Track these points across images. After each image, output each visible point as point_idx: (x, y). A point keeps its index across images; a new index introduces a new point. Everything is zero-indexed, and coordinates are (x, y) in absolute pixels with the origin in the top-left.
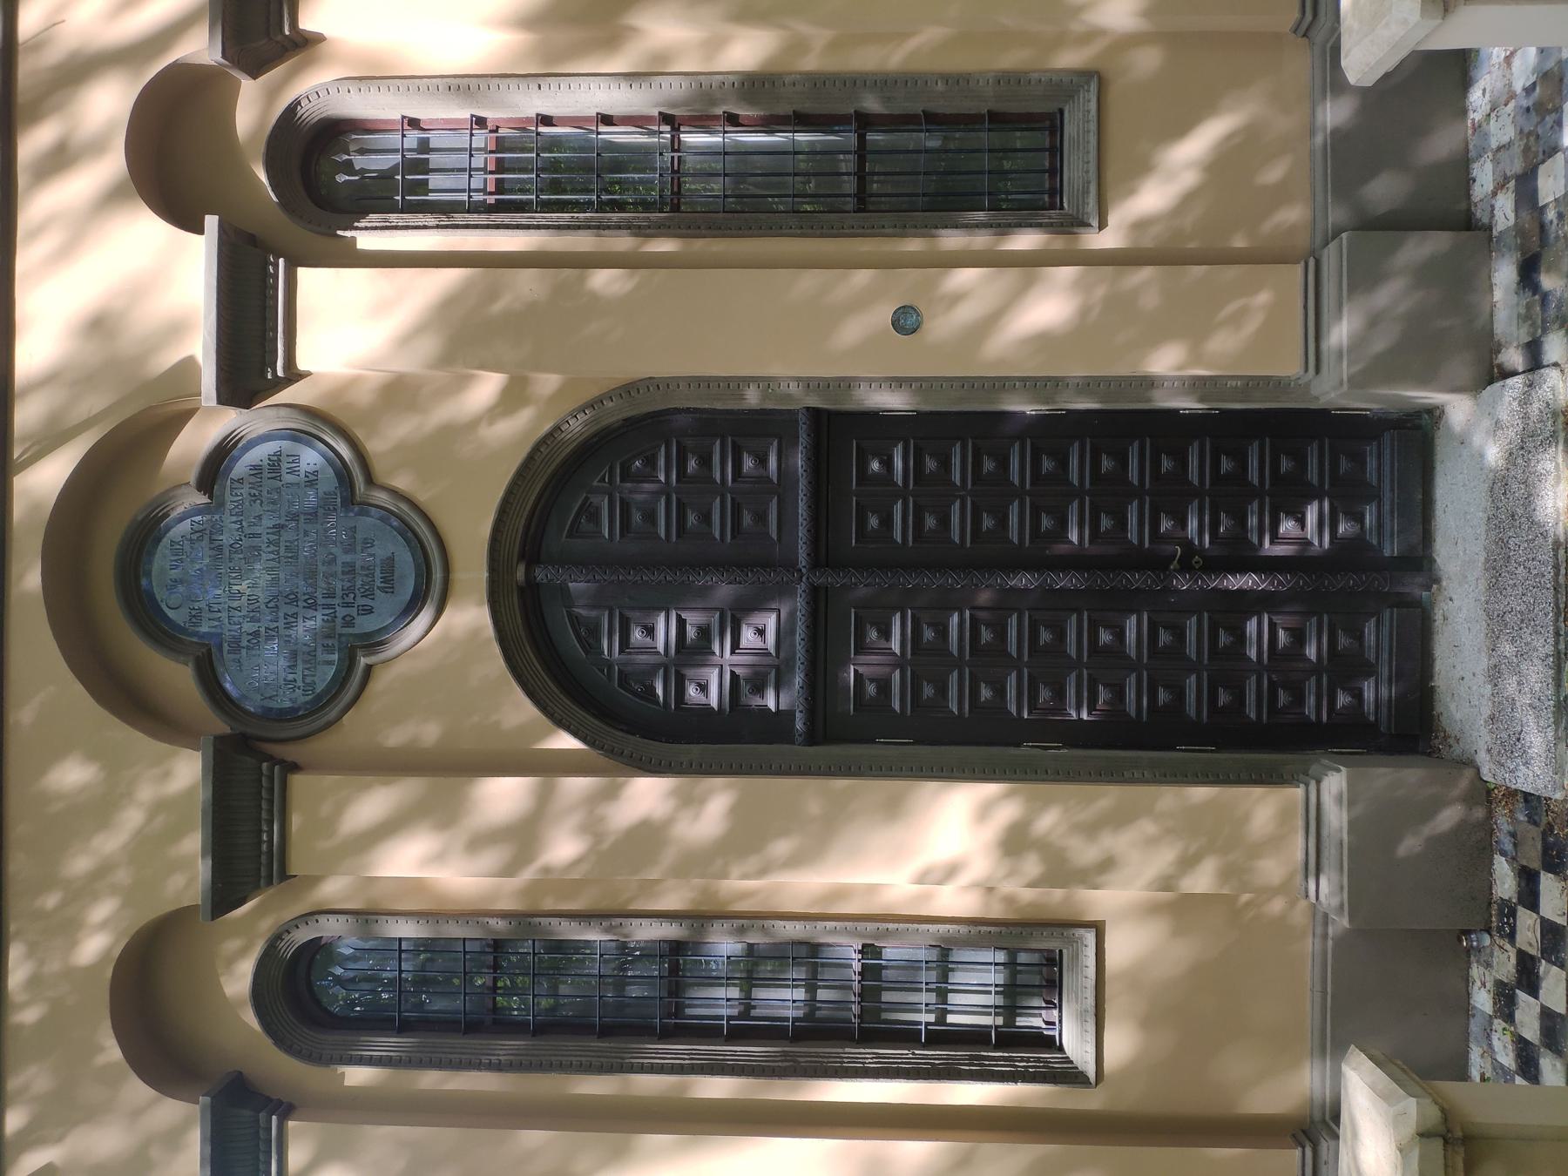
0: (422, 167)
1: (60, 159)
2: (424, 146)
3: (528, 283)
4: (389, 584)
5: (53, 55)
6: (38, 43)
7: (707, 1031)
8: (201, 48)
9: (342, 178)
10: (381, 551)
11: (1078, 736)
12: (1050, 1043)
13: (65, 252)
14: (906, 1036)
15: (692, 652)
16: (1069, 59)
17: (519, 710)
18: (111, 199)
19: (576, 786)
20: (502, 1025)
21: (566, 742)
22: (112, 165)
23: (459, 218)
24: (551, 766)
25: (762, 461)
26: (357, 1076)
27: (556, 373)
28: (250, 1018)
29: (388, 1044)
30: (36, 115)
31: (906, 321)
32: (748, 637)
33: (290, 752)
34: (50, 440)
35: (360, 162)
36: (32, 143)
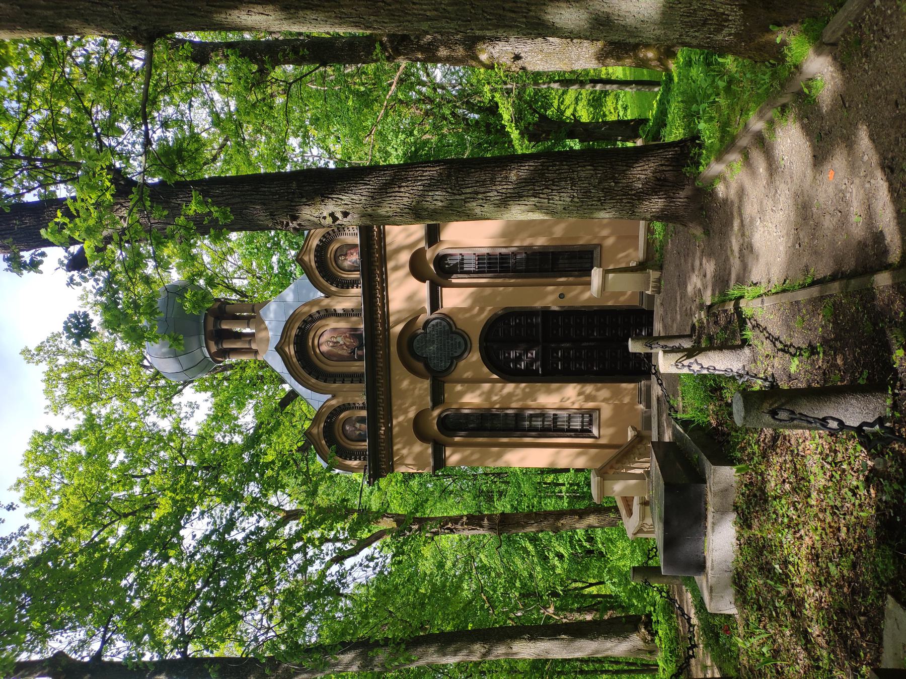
0: (463, 264)
1: (396, 268)
2: (463, 259)
3: (488, 290)
4: (460, 347)
5: (393, 247)
6: (390, 244)
7: (524, 430)
8: (423, 244)
9: (498, 299)
10: (458, 341)
11: (597, 373)
12: (591, 432)
13: (399, 285)
14: (562, 430)
15: (518, 359)
16: (595, 242)
17: (485, 370)
18: (407, 276)
19: (499, 385)
20: (485, 430)
21: (495, 376)
22: (407, 269)
23: (472, 275)
24: (493, 381)
25: (580, 365)
26: (457, 439)
27: (28, 203)
28: (436, 427)
29: (463, 433)
30: (390, 259)
31: (562, 296)
32: (529, 355)
33: (443, 379)
34: (397, 323)
35: (449, 262)
36: (390, 265)
